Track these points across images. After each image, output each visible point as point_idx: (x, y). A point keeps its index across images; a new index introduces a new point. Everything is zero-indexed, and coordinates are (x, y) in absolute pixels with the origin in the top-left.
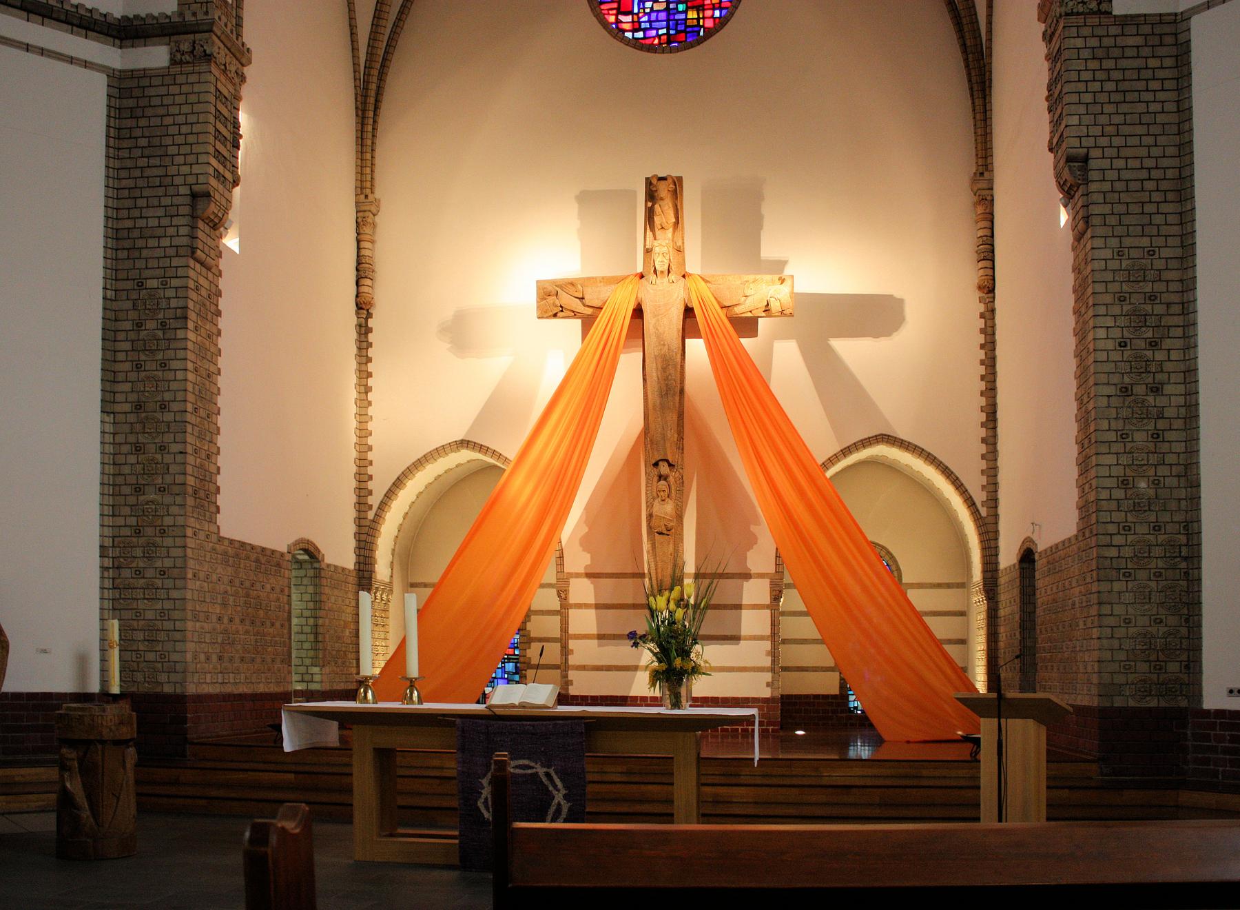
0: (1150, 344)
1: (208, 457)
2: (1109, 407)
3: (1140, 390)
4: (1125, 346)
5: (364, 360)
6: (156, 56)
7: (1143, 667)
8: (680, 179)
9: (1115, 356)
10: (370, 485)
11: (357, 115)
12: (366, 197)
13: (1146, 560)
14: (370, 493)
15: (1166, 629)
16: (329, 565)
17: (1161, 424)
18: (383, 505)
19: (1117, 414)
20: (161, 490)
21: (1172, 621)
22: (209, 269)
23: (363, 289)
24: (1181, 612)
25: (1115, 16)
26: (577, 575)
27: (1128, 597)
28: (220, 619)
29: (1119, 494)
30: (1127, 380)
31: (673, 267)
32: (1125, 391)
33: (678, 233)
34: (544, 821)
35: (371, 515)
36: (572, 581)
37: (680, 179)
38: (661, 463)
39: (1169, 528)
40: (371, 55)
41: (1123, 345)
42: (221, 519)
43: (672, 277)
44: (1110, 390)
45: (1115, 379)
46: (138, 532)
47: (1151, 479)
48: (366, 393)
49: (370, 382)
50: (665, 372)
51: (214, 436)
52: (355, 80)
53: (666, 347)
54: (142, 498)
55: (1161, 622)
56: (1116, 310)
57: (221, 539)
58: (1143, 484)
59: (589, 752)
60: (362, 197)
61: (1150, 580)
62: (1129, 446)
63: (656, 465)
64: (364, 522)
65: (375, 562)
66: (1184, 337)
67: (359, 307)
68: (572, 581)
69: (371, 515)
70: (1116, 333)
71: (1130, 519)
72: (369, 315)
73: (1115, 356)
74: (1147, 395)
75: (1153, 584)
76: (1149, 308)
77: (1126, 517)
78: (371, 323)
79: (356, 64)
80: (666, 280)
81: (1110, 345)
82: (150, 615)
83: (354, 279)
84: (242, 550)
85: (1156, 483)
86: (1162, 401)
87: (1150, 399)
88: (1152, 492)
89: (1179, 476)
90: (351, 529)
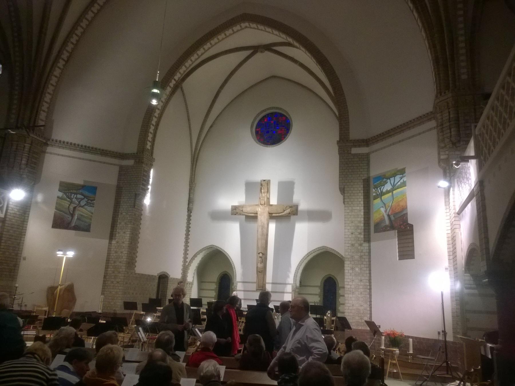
0: (360, 233)
1: (134, 254)
2: (348, 249)
3: (357, 245)
4: (353, 234)
5: (189, 223)
6: (130, 162)
7: (357, 318)
8: (269, 181)
9: (350, 236)
10: (188, 256)
11: (191, 163)
12: (192, 183)
13: (358, 289)
14: (187, 258)
15: (363, 308)
16: (171, 278)
17: (362, 254)
18: (191, 261)
19: (350, 251)
20: (120, 262)
21: (365, 306)
22: (139, 210)
23: (190, 206)
24: (368, 304)
25: (352, 154)
26: (240, 282)
27: (353, 299)
28: (133, 294)
29: (351, 271)
30: (353, 242)
31: (265, 203)
32: (353, 245)
33: (268, 194)
34: (428, 356)
35: (187, 264)
36: (238, 283)
37: (269, 181)
38: (260, 253)
39: (364, 281)
40: (196, 149)
41: (352, 234)
42: (136, 269)
43: (265, 205)
44: (349, 245)
45: (350, 242)
46: (113, 272)
47: (359, 268)
48: (189, 232)
49: (190, 229)
50: (262, 230)
51: (136, 249)
52: (191, 155)
53: (263, 223)
54: (115, 264)
55: (362, 306)
56: (351, 225)
57: (135, 274)
58: (357, 269)
59: (148, 335)
60: (191, 183)
61: (359, 294)
62: (353, 259)
63: (259, 254)
64: (185, 266)
65: (187, 277)
66: (183, 279)
67: (188, 210)
68: (238, 283)
69: (187, 264)
70: (350, 231)
71: (353, 278)
72: (191, 212)
73: (350, 236)
74: (358, 246)
75: (360, 296)
76: (359, 224)
77: (352, 278)
78: (191, 214)
79: (192, 151)
80: (263, 206)
81: (349, 233)
82: (113, 293)
83: (188, 203)
84: (142, 276)
85: (361, 269)
86: (362, 248)
87: (359, 247)
88: (359, 271)
89: (367, 267)
90: (181, 267)
